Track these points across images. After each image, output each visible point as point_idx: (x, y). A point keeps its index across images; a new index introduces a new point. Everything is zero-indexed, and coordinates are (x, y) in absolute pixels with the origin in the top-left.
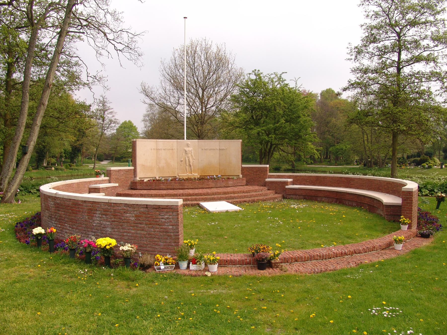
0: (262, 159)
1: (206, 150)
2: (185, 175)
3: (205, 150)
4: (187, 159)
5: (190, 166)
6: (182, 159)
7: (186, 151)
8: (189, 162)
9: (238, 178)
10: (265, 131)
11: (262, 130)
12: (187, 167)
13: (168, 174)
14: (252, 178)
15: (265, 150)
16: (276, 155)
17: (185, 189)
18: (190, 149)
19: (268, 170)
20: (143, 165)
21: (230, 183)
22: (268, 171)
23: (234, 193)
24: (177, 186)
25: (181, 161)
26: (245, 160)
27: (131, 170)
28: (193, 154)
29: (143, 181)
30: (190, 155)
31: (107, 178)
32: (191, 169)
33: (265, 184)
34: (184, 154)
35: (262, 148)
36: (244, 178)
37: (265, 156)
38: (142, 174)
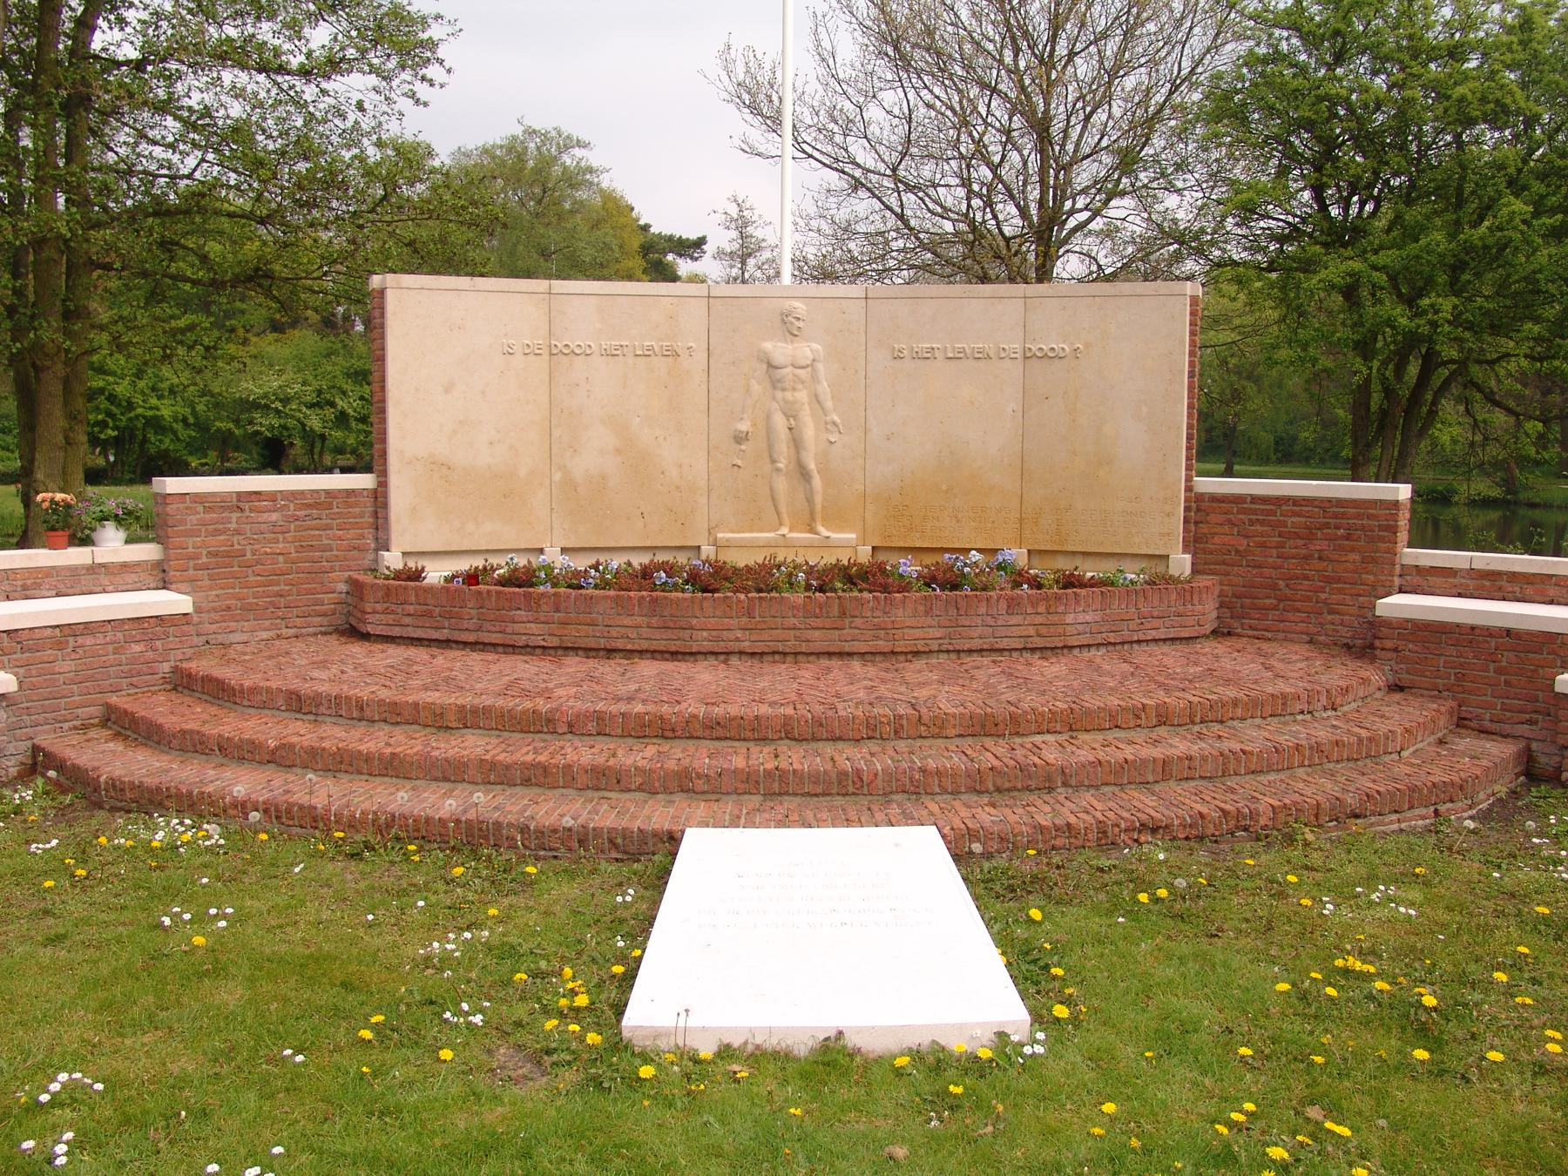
0: (1368, 445)
1: (927, 356)
2: (744, 543)
3: (917, 357)
4: (780, 422)
5: (804, 474)
6: (744, 427)
7: (771, 366)
8: (797, 443)
9: (1160, 582)
10: (1393, 279)
11: (1375, 268)
12: (781, 484)
13: (633, 534)
14: (1267, 581)
15: (1388, 392)
16: (1450, 429)
17: (693, 655)
18: (805, 350)
19: (1403, 521)
20: (439, 467)
21: (1080, 617)
22: (1403, 536)
23: (1073, 723)
24: (632, 627)
25: (740, 439)
26: (1216, 441)
27: (350, 493)
28: (824, 388)
29: (417, 575)
30: (802, 395)
31: (147, 552)
32: (810, 500)
33: (1369, 641)
34: (756, 388)
35: (1368, 380)
36: (1204, 581)
37: (1376, 431)
38: (431, 529)
